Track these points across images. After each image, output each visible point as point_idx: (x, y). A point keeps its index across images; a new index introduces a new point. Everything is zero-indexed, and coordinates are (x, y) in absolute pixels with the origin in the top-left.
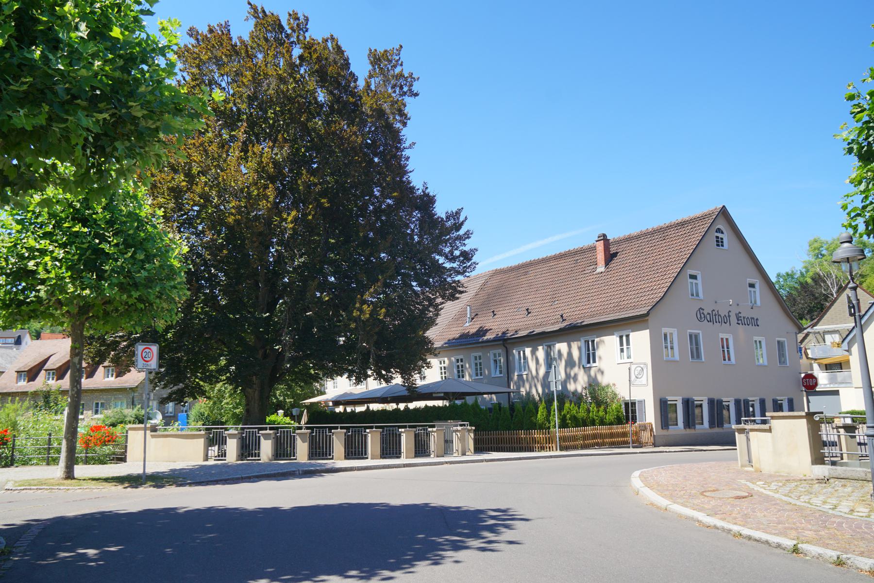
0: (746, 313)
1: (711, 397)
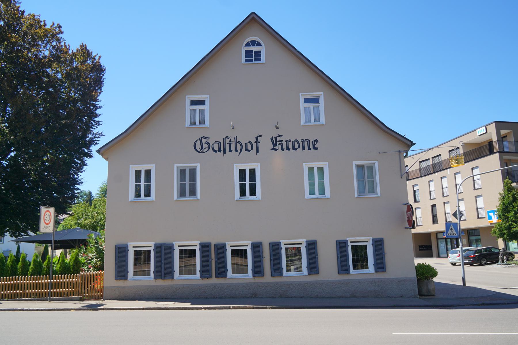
0: (288, 134)
1: (206, 240)
